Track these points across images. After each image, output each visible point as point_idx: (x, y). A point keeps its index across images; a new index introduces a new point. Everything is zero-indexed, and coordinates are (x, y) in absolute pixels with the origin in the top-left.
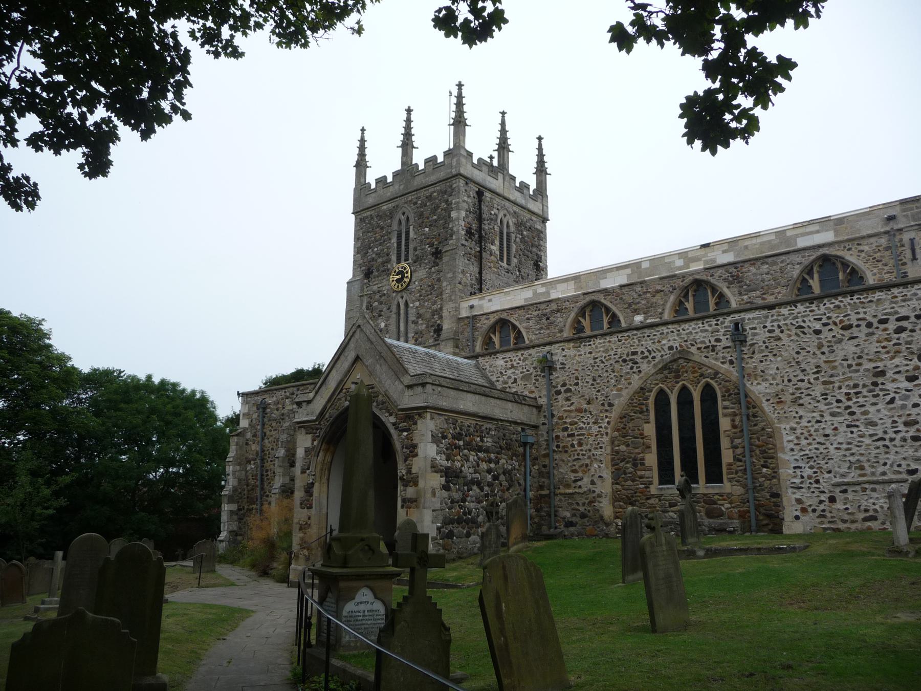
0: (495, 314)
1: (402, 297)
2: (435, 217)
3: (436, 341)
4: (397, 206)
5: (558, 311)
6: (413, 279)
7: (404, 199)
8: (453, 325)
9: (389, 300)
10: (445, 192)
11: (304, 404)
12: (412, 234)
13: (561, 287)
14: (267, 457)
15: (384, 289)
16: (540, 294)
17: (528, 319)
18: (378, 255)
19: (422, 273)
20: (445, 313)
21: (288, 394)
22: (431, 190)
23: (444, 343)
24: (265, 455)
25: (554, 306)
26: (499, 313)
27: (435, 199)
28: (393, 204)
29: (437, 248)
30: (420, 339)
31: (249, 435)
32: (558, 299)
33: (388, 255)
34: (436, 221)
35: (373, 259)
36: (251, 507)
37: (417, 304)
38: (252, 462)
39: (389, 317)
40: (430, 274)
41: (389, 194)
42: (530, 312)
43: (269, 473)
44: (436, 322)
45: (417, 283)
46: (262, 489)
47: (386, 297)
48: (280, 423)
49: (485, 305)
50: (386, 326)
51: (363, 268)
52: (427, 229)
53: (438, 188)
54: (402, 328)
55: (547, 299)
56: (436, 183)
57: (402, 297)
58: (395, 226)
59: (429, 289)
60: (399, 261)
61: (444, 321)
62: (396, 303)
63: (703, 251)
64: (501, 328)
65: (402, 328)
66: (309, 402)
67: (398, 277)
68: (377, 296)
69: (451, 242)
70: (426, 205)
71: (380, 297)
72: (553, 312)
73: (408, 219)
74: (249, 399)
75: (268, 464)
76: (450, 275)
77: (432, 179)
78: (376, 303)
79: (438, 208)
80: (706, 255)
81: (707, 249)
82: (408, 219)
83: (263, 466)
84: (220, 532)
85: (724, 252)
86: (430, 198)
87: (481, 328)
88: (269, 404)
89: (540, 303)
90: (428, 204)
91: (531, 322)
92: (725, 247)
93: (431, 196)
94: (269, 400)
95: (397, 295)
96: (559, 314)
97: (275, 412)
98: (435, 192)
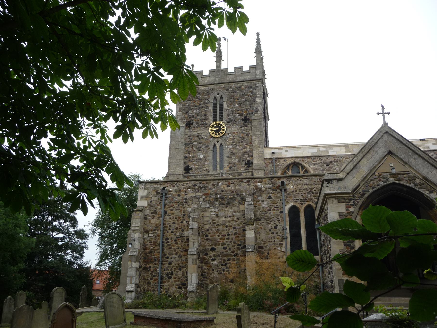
0: (291, 159)
1: (218, 142)
2: (243, 100)
3: (246, 169)
4: (213, 89)
5: (335, 162)
6: (228, 132)
7: (218, 86)
8: (261, 161)
9: (207, 142)
10: (251, 87)
11: (334, 181)
12: (225, 106)
13: (335, 149)
14: (167, 229)
15: (202, 135)
16: (322, 151)
17: (314, 164)
18: (198, 115)
19: (234, 129)
20: (255, 154)
21: (190, 185)
22: (240, 84)
23: (256, 171)
24: (166, 227)
25: (332, 159)
26: (293, 159)
27: (243, 89)
28: (210, 88)
29: (246, 117)
30: (233, 168)
31: (148, 212)
32: (335, 155)
33: (205, 115)
34: (244, 102)
35: (193, 116)
36: (148, 266)
37: (231, 147)
38: (150, 232)
39: (207, 152)
40: (240, 131)
41: (206, 81)
42: (315, 160)
43: (169, 240)
44: (246, 159)
45: (230, 134)
46: (163, 252)
47: (204, 140)
48: (183, 205)
49: (283, 153)
50: (204, 157)
51: (184, 121)
52: (237, 105)
53: (245, 84)
54: (218, 159)
55: (328, 155)
56: (245, 81)
57: (218, 142)
58: (211, 99)
59: (240, 139)
60: (215, 120)
61: (254, 159)
62: (213, 144)
63: (421, 142)
64: (292, 167)
65: (218, 159)
66: (340, 180)
67: (216, 129)
68: (197, 139)
69: (256, 115)
70: (236, 92)
71: (199, 139)
72: (331, 162)
73: (221, 97)
74: (148, 186)
75: (168, 234)
76: (258, 133)
77: (234, 79)
78: (196, 143)
79: (246, 95)
80: (424, 144)
81: (424, 142)
82: (221, 97)
83: (163, 236)
84: (361, 284)
85: (434, 144)
86: (239, 88)
87: (281, 165)
88: (170, 191)
89: (322, 156)
90: (238, 91)
91: (316, 166)
92: (434, 142)
93: (240, 87)
94: (169, 188)
95: (214, 140)
96: (335, 164)
97: (177, 197)
98: (242, 86)
